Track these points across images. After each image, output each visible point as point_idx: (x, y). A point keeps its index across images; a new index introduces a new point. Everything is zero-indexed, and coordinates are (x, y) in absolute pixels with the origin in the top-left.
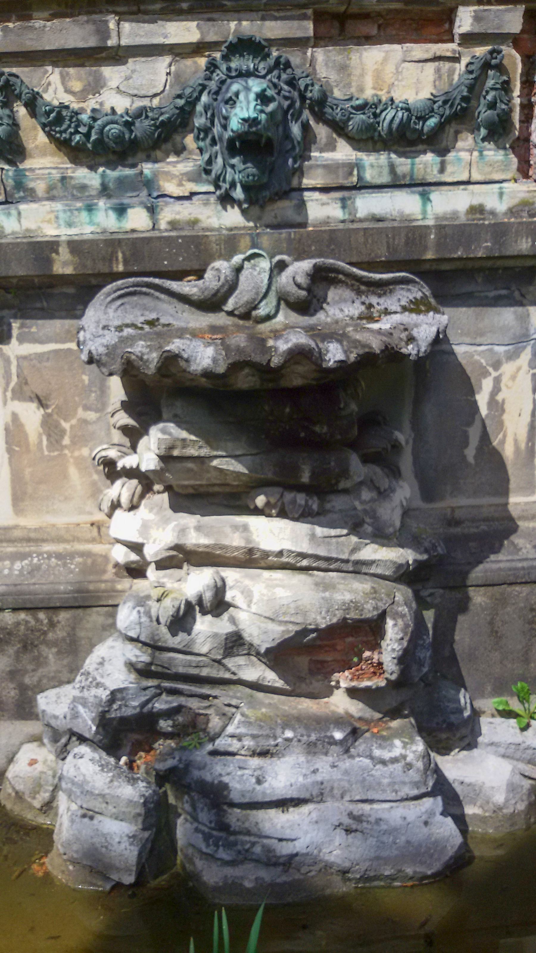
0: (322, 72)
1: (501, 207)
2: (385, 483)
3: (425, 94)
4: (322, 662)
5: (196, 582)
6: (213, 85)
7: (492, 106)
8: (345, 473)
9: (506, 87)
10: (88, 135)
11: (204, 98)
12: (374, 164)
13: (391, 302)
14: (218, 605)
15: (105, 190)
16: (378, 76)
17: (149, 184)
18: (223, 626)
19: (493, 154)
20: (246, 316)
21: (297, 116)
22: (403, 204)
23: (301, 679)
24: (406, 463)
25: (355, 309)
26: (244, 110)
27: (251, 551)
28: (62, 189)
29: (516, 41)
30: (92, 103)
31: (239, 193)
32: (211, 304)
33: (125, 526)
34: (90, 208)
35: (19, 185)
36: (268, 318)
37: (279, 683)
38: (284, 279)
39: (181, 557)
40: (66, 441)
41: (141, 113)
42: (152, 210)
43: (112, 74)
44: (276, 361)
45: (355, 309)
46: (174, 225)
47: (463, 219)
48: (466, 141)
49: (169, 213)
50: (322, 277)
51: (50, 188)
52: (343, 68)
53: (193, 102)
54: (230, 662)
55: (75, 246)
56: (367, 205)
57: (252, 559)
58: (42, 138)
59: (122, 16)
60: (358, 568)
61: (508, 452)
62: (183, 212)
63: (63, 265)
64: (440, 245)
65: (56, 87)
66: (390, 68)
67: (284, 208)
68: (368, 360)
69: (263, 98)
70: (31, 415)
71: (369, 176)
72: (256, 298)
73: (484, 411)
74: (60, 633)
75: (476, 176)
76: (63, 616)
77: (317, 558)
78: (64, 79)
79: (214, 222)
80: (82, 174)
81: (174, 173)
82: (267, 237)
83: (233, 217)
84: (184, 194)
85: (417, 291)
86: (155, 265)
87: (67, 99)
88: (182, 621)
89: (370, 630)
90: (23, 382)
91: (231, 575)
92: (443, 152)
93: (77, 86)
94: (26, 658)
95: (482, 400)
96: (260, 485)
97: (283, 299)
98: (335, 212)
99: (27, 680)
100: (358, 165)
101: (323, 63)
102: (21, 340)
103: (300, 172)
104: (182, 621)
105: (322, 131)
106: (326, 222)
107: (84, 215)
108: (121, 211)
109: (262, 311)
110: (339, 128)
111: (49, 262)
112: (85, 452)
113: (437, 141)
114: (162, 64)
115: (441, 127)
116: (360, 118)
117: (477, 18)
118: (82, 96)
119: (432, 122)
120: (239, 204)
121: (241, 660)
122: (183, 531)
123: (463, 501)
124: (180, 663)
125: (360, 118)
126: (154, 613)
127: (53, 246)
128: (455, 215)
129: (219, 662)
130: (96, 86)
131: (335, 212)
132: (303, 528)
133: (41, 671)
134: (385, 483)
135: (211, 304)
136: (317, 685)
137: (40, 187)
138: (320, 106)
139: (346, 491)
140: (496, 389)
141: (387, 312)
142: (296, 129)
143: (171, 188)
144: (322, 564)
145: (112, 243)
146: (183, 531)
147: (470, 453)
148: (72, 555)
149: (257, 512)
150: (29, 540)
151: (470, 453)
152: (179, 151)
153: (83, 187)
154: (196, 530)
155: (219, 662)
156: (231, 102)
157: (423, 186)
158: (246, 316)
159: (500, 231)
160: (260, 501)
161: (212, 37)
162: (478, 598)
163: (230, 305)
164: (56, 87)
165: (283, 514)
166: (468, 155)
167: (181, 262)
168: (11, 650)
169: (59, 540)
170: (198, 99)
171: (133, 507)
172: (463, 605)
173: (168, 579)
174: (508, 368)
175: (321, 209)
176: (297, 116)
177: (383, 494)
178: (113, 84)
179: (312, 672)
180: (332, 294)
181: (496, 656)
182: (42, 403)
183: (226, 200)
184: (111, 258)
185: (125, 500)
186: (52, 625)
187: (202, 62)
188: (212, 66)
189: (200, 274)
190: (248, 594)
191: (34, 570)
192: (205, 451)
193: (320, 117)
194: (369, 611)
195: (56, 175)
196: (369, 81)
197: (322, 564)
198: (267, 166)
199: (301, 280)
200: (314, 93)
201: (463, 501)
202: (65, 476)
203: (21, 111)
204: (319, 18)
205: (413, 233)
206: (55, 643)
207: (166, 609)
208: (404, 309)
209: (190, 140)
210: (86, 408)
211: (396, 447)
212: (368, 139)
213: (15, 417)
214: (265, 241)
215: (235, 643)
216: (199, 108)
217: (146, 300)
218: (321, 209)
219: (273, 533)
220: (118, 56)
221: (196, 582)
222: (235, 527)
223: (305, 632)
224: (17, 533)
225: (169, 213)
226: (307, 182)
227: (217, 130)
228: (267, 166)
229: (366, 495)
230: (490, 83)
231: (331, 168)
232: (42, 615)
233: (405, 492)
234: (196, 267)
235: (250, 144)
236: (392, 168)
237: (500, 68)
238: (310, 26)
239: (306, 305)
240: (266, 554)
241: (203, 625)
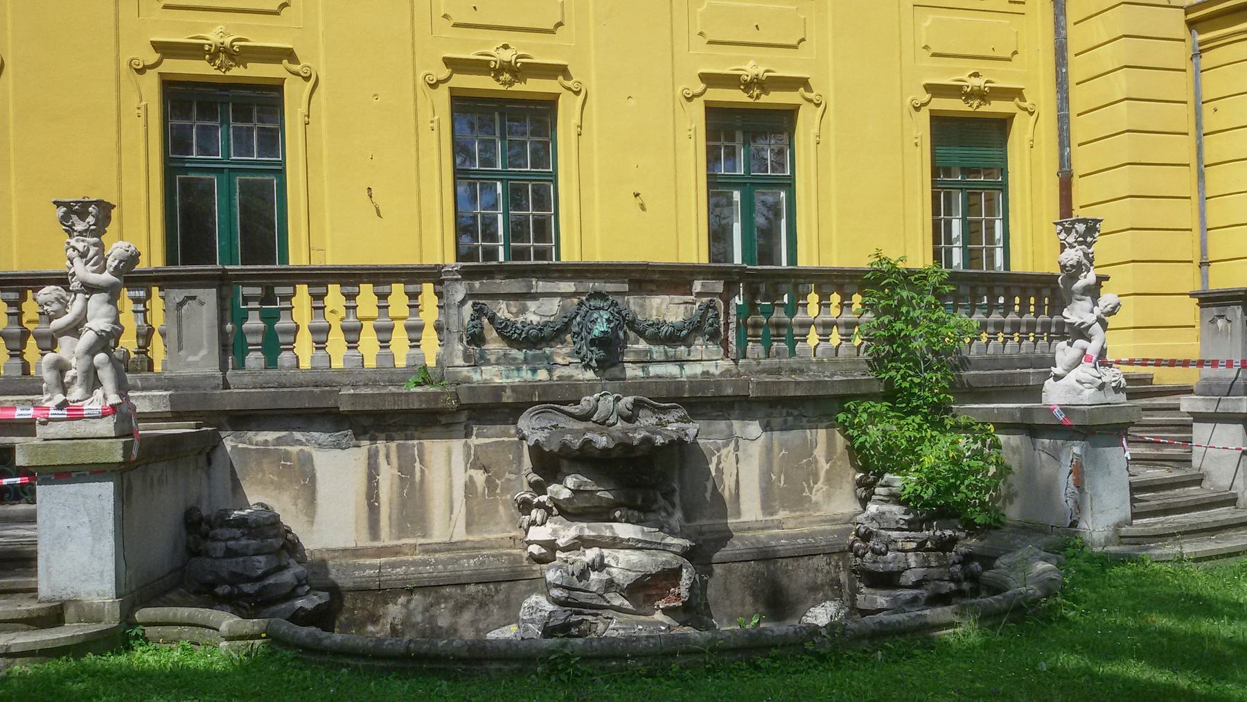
0: (632, 307)
1: (717, 372)
2: (670, 510)
3: (680, 319)
4: (650, 596)
5: (591, 554)
6: (582, 313)
7: (711, 325)
8: (655, 501)
9: (717, 316)
10: (520, 335)
11: (578, 319)
12: (658, 351)
13: (669, 417)
14: (600, 565)
15: (526, 361)
16: (658, 309)
17: (549, 358)
18: (604, 576)
19: (712, 347)
20: (603, 423)
21: (621, 328)
22: (673, 370)
23: (640, 606)
24: (677, 500)
25: (654, 421)
26: (600, 328)
27: (615, 538)
28: (504, 360)
29: (720, 295)
30: (521, 318)
31: (594, 363)
32: (585, 417)
33: (537, 533)
34: (518, 369)
35: (482, 357)
36: (614, 424)
37: (631, 607)
38: (621, 404)
39: (581, 543)
40: (498, 491)
41: (546, 324)
42: (550, 371)
43: (532, 305)
44: (635, 443)
45: (654, 421)
46: (560, 378)
47: (699, 379)
48: (699, 341)
49: (558, 373)
50: (638, 405)
51: (498, 359)
52: (642, 306)
53: (571, 319)
54: (607, 596)
55: (514, 388)
56: (654, 370)
57: (616, 543)
58: (495, 334)
59: (538, 279)
60: (665, 548)
61: (726, 495)
62: (566, 371)
63: (508, 398)
64: (691, 390)
65: (503, 310)
66: (664, 306)
67: (615, 371)
68: (672, 442)
69: (608, 321)
70: (480, 477)
71: (655, 356)
72: (606, 418)
73: (714, 474)
74: (501, 596)
75: (705, 357)
76: (503, 586)
77: (646, 542)
78: (507, 306)
79: (581, 377)
80: (514, 352)
81: (561, 353)
82: (609, 385)
83: (590, 374)
84: (566, 364)
85: (682, 412)
86: (555, 399)
87: (509, 316)
88: (583, 575)
89: (672, 575)
90: (477, 458)
91: (606, 552)
92: (689, 346)
93: (514, 310)
94: (481, 612)
95: (712, 467)
96: (617, 505)
97: (622, 416)
98: (640, 373)
99: (481, 626)
100: (650, 351)
101: (633, 303)
102: (477, 437)
103: (623, 354)
104: (583, 575)
105: (632, 335)
106: (635, 378)
107: (515, 373)
108: (534, 371)
109: (611, 421)
110: (641, 334)
111: (500, 396)
112: (509, 497)
113: (686, 341)
114: (556, 301)
115: (688, 334)
116: (651, 330)
117: (703, 285)
118: (516, 315)
119: (684, 332)
120: (594, 369)
121: (612, 595)
122: (582, 529)
123: (705, 522)
124: (582, 597)
125: (651, 330)
126: (570, 571)
127: (502, 388)
128: (695, 376)
129: (601, 596)
130: (524, 310)
131: (640, 373)
132: (638, 528)
133: (489, 620)
134: (670, 510)
135: (585, 417)
136: (648, 609)
137: (493, 358)
138: (632, 324)
139: (653, 511)
140: (719, 463)
141: (669, 422)
142: (621, 334)
143: (559, 360)
144: (648, 546)
145: (533, 387)
146: (582, 529)
147: (708, 495)
148: (501, 555)
149: (615, 520)
150: (474, 548)
151: (708, 495)
152: (563, 342)
153: (516, 359)
154: (588, 529)
155: (601, 596)
156: (594, 322)
157: (680, 362)
158: (603, 423)
159: (718, 384)
160: (618, 514)
161: (581, 290)
162: (718, 570)
163: (595, 418)
164: (503, 310)
165: (627, 521)
166: (700, 347)
167: (567, 397)
168: (473, 608)
169: (492, 548)
170: (575, 318)
171: (543, 523)
172: (710, 573)
173: (572, 556)
174: (724, 451)
175: (632, 371)
176: (621, 328)
177: (670, 515)
178: (532, 310)
179: (645, 602)
180: (641, 413)
181: (727, 602)
182: (486, 471)
183: (587, 366)
184: (532, 394)
185: (539, 520)
186: (497, 591)
187: (576, 301)
188: (581, 304)
189: (577, 402)
190: (616, 559)
191: (482, 563)
192: (594, 488)
193: (632, 328)
194: (675, 565)
195: (501, 353)
196: (654, 312)
197: (648, 546)
198: (608, 353)
199: (630, 406)
200: (630, 317)
201: (705, 522)
202: (497, 511)
203: (486, 321)
204: (631, 282)
205: (678, 385)
206: (498, 602)
207: (577, 568)
208: (677, 421)
209: (568, 337)
210: (510, 472)
211: (674, 490)
212: (655, 339)
213: (471, 477)
214: (608, 387)
215: (610, 584)
216: (574, 322)
217: (550, 415)
218: (632, 371)
219: (625, 530)
220: (535, 297)
221: (591, 554)
222: (607, 527)
223: (645, 576)
224: (468, 545)
225: (558, 373)
226: (625, 358)
227: (584, 334)
228: (608, 353)
229: (663, 514)
230: (710, 315)
231: (637, 352)
232: (491, 586)
233: (678, 515)
234: (574, 398)
235: (602, 342)
236: (666, 352)
237: (714, 308)
238: (627, 286)
239: (629, 419)
240: (622, 540)
241: (594, 576)
